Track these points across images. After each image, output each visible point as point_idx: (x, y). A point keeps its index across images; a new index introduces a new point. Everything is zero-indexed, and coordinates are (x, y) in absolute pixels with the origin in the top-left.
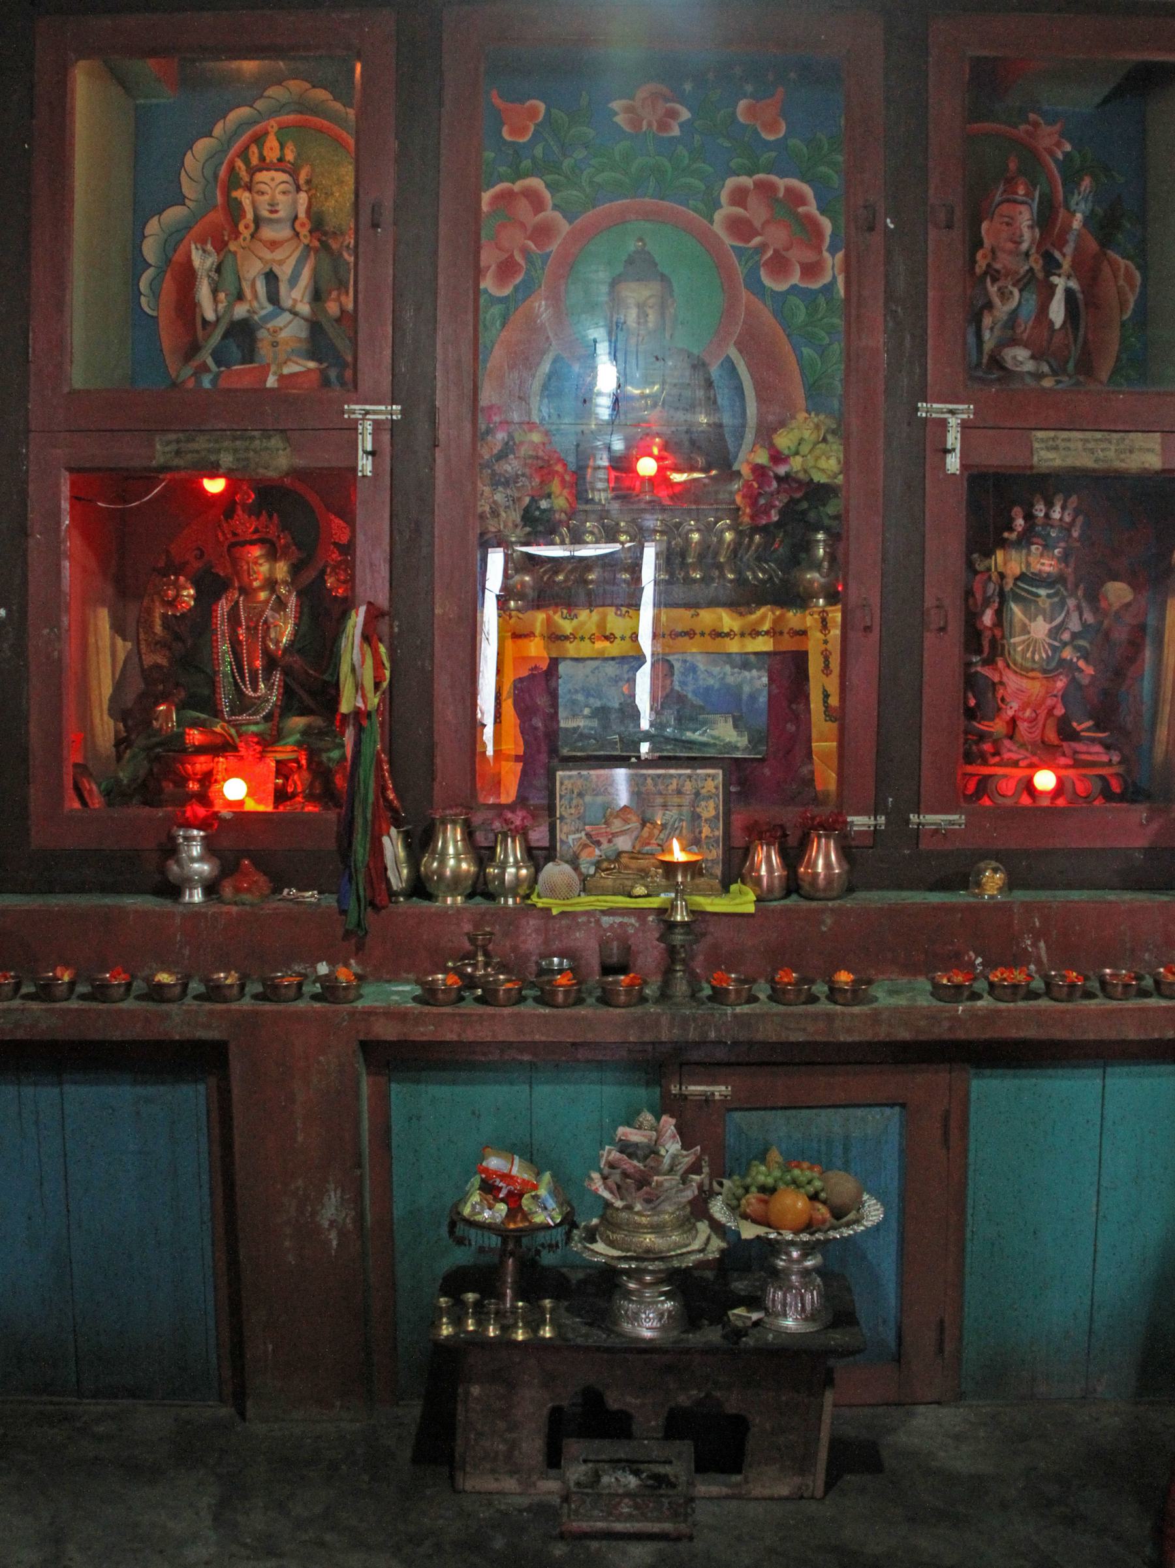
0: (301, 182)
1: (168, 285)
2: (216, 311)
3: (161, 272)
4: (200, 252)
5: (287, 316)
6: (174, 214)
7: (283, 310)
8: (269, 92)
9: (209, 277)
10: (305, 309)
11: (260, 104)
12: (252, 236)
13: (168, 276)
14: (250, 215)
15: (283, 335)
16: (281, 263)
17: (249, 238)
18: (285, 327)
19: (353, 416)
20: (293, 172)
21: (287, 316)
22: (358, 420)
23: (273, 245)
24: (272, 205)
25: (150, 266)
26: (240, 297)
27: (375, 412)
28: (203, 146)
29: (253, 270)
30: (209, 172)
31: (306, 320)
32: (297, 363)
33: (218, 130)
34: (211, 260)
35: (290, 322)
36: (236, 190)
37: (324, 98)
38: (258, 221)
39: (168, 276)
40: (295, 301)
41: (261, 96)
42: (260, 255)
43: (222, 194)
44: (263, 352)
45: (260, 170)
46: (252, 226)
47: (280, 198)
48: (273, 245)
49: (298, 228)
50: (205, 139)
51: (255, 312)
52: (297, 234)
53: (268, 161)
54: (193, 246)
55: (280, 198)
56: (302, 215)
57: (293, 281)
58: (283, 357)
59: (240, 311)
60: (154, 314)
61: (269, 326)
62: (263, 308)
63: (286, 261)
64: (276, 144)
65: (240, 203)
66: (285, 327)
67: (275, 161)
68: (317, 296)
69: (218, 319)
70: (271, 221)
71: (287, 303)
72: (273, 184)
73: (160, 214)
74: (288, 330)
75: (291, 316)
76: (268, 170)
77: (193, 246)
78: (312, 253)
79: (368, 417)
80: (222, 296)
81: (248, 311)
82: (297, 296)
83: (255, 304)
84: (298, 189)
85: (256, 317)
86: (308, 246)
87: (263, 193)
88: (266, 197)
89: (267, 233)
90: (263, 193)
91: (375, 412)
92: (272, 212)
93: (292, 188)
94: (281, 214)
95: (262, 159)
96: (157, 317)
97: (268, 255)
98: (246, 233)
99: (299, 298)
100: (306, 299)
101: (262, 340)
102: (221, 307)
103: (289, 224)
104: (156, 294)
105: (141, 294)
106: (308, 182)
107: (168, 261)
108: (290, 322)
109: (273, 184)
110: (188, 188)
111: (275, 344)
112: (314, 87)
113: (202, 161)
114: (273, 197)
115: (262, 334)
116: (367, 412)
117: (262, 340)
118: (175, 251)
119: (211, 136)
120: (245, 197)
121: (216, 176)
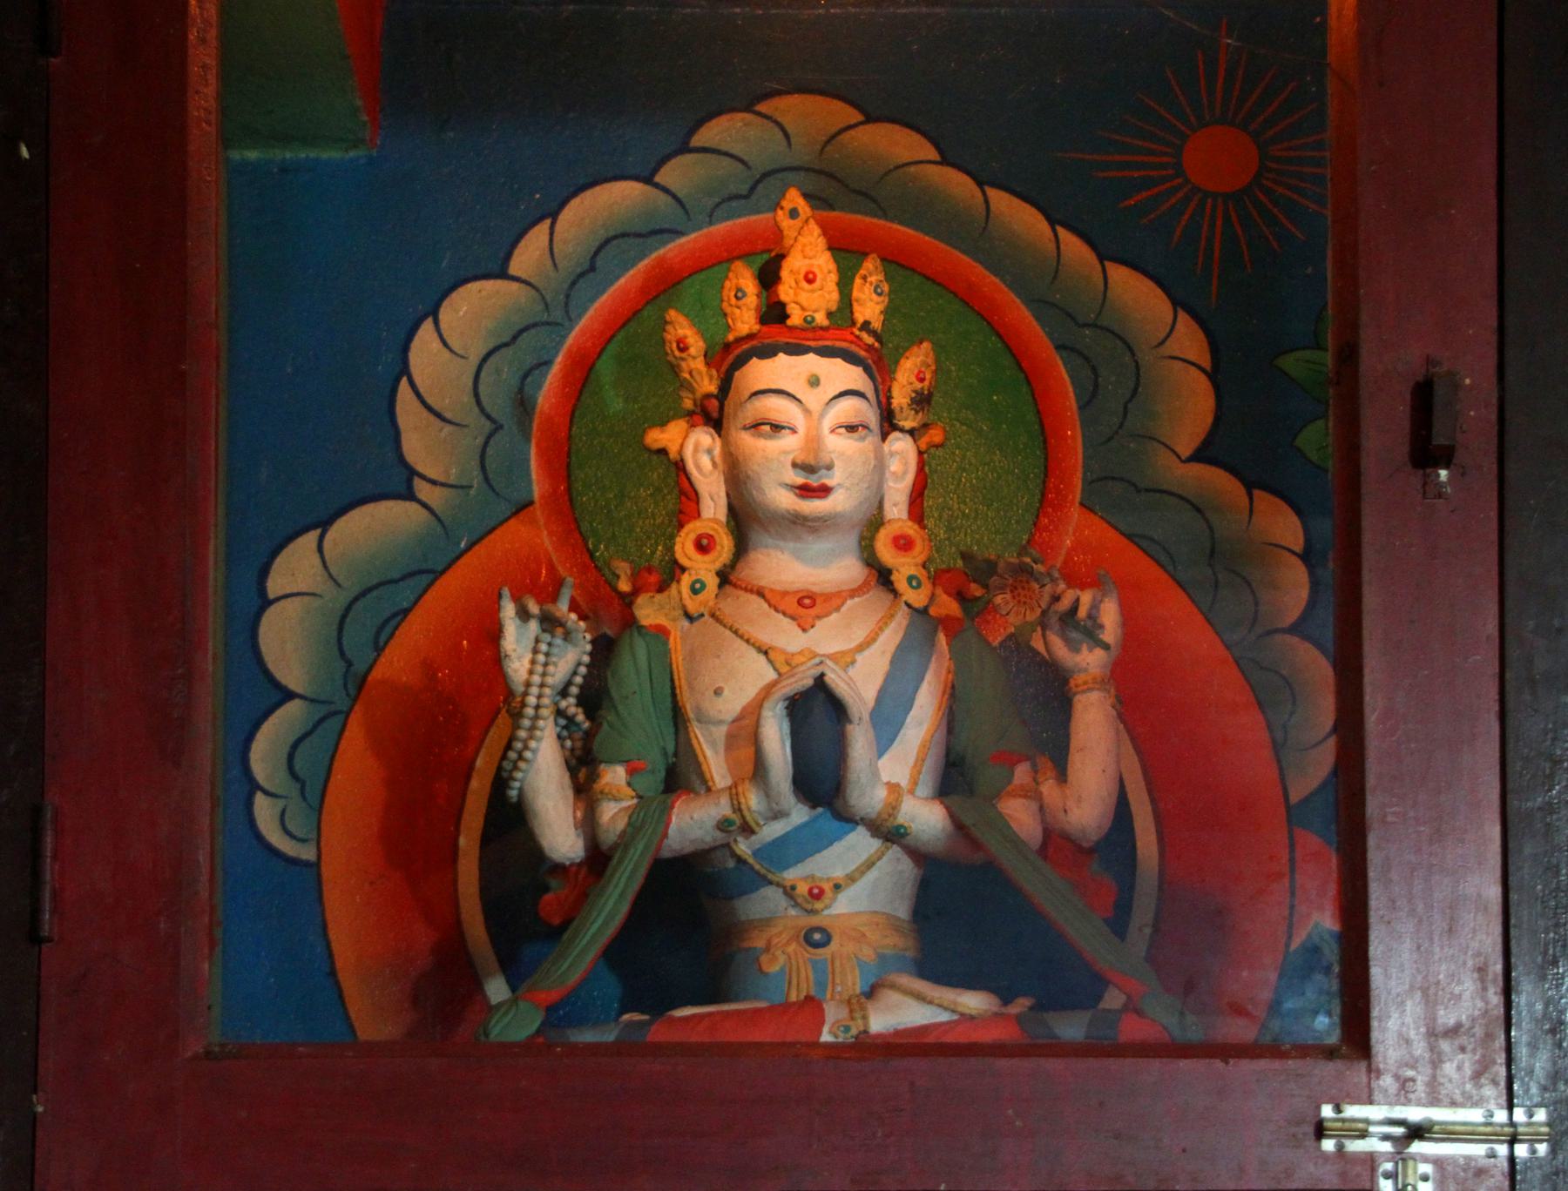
0: (900, 398)
1: (357, 771)
2: (588, 824)
3: (328, 717)
4: (534, 626)
5: (860, 843)
6: (372, 529)
7: (848, 819)
8: (713, 133)
9: (560, 713)
10: (926, 818)
11: (677, 173)
12: (725, 578)
13: (355, 731)
14: (714, 507)
15: (842, 906)
16: (846, 659)
17: (712, 582)
18: (851, 879)
19: (1355, 1146)
20: (878, 366)
21: (860, 843)
22: (1371, 1160)
23: (806, 606)
24: (809, 469)
25: (289, 695)
26: (680, 776)
27: (1451, 1134)
28: (473, 310)
29: (736, 682)
30: (499, 402)
31: (918, 855)
32: (921, 998)
33: (529, 255)
34: (570, 659)
35: (869, 865)
36: (663, 423)
37: (904, 155)
38: (746, 520)
39: (355, 731)
40: (893, 788)
41: (685, 149)
42: (765, 637)
43: (546, 460)
44: (774, 966)
45: (768, 352)
46: (725, 545)
47: (839, 446)
48: (806, 606)
49: (886, 554)
50: (489, 286)
51: (747, 830)
52: (883, 577)
53: (796, 319)
54: (508, 610)
55: (839, 446)
56: (896, 508)
57: (888, 720)
58: (855, 982)
59: (692, 823)
60: (307, 853)
61: (791, 875)
62: (778, 815)
63: (859, 652)
64: (823, 262)
65: (680, 466)
66: (851, 879)
67: (821, 319)
68: (954, 776)
69: (598, 859)
70: (799, 524)
71: (868, 796)
72: (814, 399)
73: (325, 524)
74: (858, 886)
75: (876, 844)
76: (796, 350)
77: (508, 610)
78: (941, 638)
79: (1417, 1147)
80: (614, 776)
81: (723, 825)
82: (894, 770)
83: (753, 800)
84: (888, 422)
85: (743, 847)
86: (924, 612)
87: (777, 428)
88: (788, 444)
89: (782, 565)
90: (777, 428)
91: (1451, 1134)
92: (805, 491)
93: (871, 416)
94: (837, 502)
95: (774, 313)
96: (316, 866)
97: (786, 636)
98: (703, 569)
99: (904, 783)
100: (926, 787)
101: (767, 922)
102: (613, 814)
103: (852, 540)
104: (309, 784)
105: (254, 787)
106: (921, 401)
107: (358, 684)
108: (869, 865)
109: (814, 399)
110: (420, 443)
111: (816, 938)
112: (870, 119)
113: (476, 352)
114: (814, 442)
115: (765, 903)
116: (1417, 1132)
117: (767, 922)
118: (379, 649)
119: (503, 275)
120: (699, 450)
121: (523, 404)
